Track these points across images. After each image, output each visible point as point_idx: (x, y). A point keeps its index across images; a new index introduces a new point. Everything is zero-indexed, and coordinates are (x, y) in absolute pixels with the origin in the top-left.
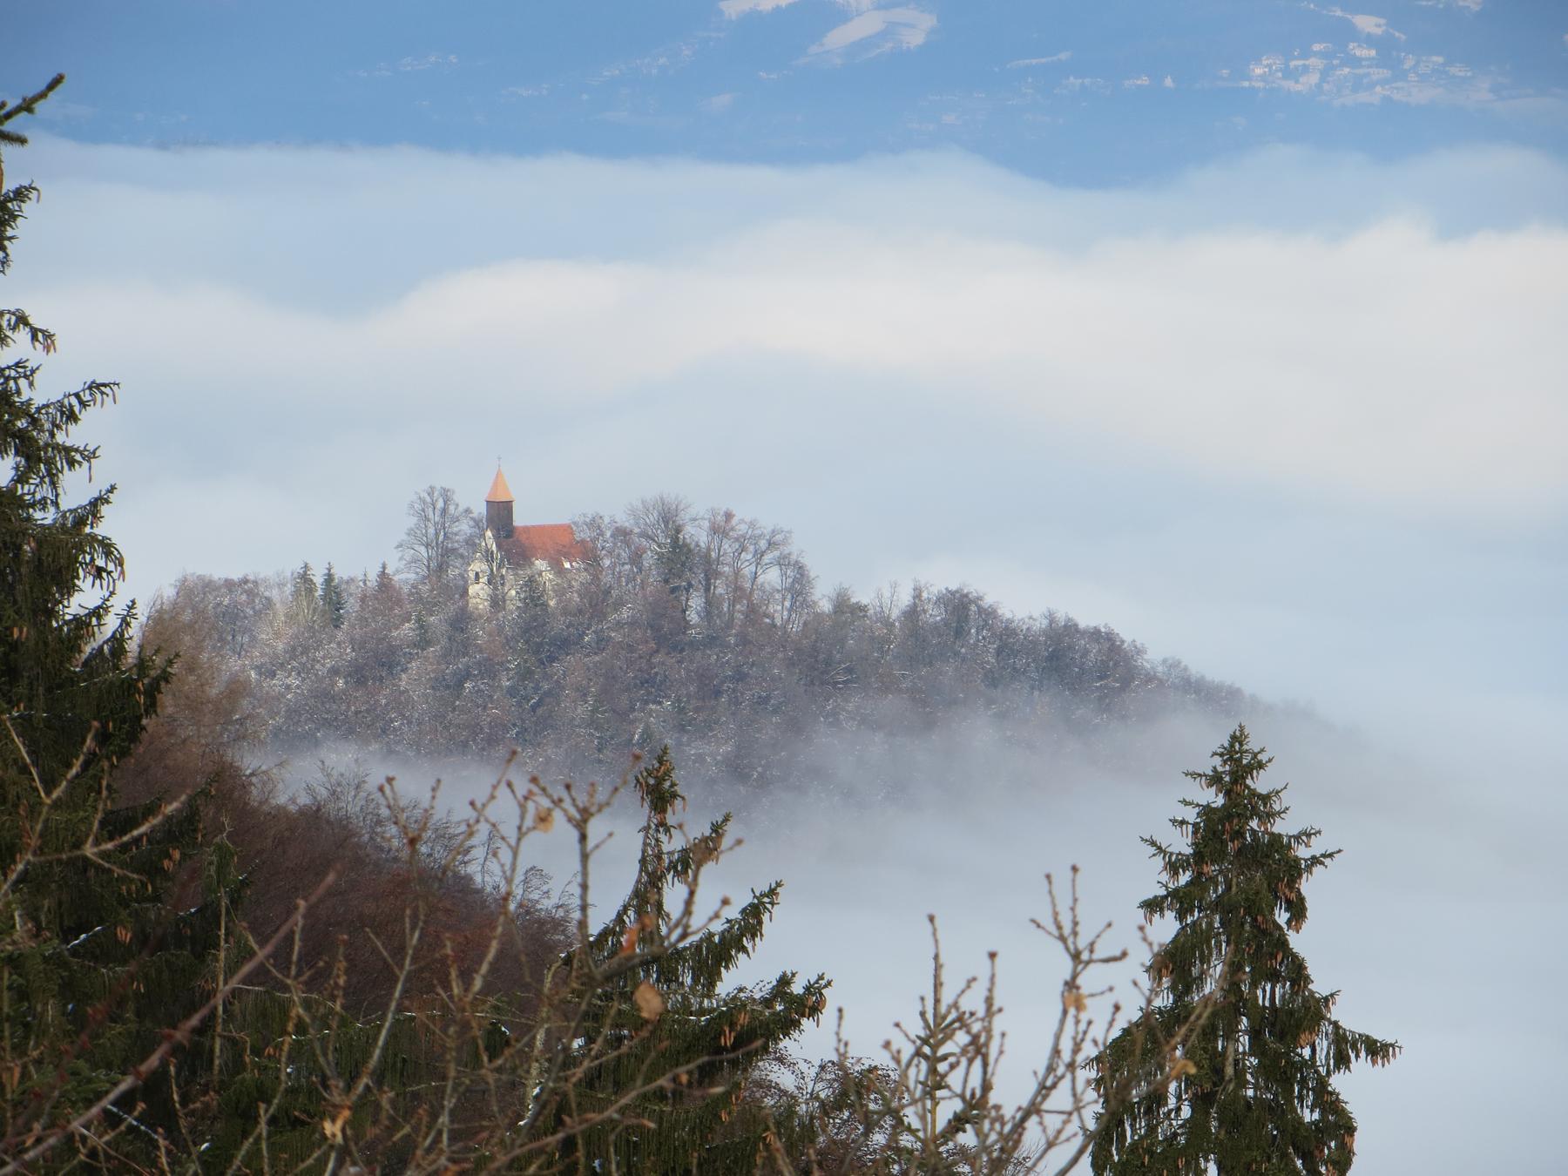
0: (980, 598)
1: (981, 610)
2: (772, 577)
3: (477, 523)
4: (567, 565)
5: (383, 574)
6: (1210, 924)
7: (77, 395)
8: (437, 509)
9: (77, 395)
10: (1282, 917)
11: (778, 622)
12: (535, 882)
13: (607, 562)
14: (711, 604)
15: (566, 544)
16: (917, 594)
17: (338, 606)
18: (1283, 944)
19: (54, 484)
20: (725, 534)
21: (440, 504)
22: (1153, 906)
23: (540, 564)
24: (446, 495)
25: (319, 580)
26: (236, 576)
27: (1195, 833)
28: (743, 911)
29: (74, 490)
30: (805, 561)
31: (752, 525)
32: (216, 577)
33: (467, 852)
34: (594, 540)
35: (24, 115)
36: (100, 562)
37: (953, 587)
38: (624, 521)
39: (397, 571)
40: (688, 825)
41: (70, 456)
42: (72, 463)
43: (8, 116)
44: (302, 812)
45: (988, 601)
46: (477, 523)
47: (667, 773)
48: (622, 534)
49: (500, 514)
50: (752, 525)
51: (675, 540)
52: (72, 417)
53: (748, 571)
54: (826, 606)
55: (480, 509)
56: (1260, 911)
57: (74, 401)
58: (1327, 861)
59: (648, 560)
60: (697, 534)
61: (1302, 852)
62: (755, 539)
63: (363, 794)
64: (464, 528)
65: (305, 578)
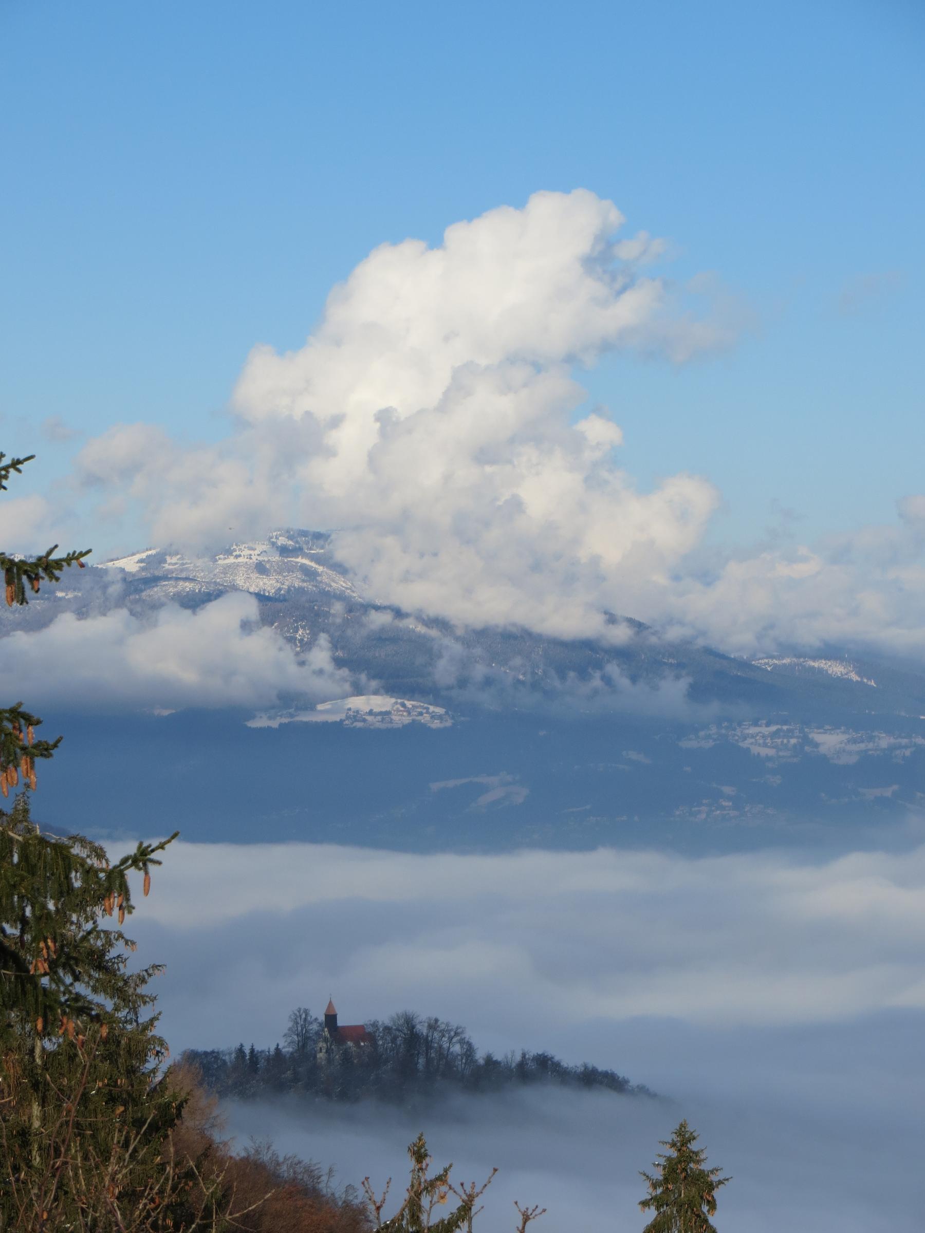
0: (552, 1058)
1: (553, 1063)
2: (457, 1049)
3: (320, 1024)
4: (362, 1044)
5: (277, 1049)
6: (672, 1212)
7: (146, 971)
8: (302, 1018)
9: (146, 971)
10: (705, 1208)
11: (460, 1069)
12: (350, 1191)
13: (381, 1042)
14: (429, 1061)
15: (359, 1033)
16: (524, 1055)
17: (256, 1063)
18: (706, 1221)
19: (136, 1014)
20: (435, 1029)
21: (303, 1016)
22: (645, 1204)
23: (350, 1044)
24: (306, 1012)
25: (247, 1051)
26: (209, 1050)
27: (664, 1169)
28: (458, 1209)
29: (145, 1014)
30: (471, 1041)
31: (447, 1025)
32: (200, 1050)
33: (319, 1177)
34: (375, 1032)
35: (160, 850)
36: (158, 1049)
37: (540, 1053)
38: (388, 1022)
39: (284, 1047)
40: (433, 1169)
41: (144, 999)
42: (145, 1003)
43: (153, 851)
44: (242, 1159)
45: (556, 1059)
46: (320, 1024)
47: (423, 1145)
48: (387, 1029)
49: (331, 1018)
50: (447, 1025)
51: (412, 1032)
52: (143, 981)
53: (446, 1046)
54: (481, 1062)
55: (322, 1018)
56: (695, 1206)
57: (145, 973)
58: (726, 1182)
59: (399, 1041)
60: (422, 1029)
61: (714, 1178)
62: (449, 1031)
63: (270, 1152)
64: (315, 1027)
65: (240, 1051)
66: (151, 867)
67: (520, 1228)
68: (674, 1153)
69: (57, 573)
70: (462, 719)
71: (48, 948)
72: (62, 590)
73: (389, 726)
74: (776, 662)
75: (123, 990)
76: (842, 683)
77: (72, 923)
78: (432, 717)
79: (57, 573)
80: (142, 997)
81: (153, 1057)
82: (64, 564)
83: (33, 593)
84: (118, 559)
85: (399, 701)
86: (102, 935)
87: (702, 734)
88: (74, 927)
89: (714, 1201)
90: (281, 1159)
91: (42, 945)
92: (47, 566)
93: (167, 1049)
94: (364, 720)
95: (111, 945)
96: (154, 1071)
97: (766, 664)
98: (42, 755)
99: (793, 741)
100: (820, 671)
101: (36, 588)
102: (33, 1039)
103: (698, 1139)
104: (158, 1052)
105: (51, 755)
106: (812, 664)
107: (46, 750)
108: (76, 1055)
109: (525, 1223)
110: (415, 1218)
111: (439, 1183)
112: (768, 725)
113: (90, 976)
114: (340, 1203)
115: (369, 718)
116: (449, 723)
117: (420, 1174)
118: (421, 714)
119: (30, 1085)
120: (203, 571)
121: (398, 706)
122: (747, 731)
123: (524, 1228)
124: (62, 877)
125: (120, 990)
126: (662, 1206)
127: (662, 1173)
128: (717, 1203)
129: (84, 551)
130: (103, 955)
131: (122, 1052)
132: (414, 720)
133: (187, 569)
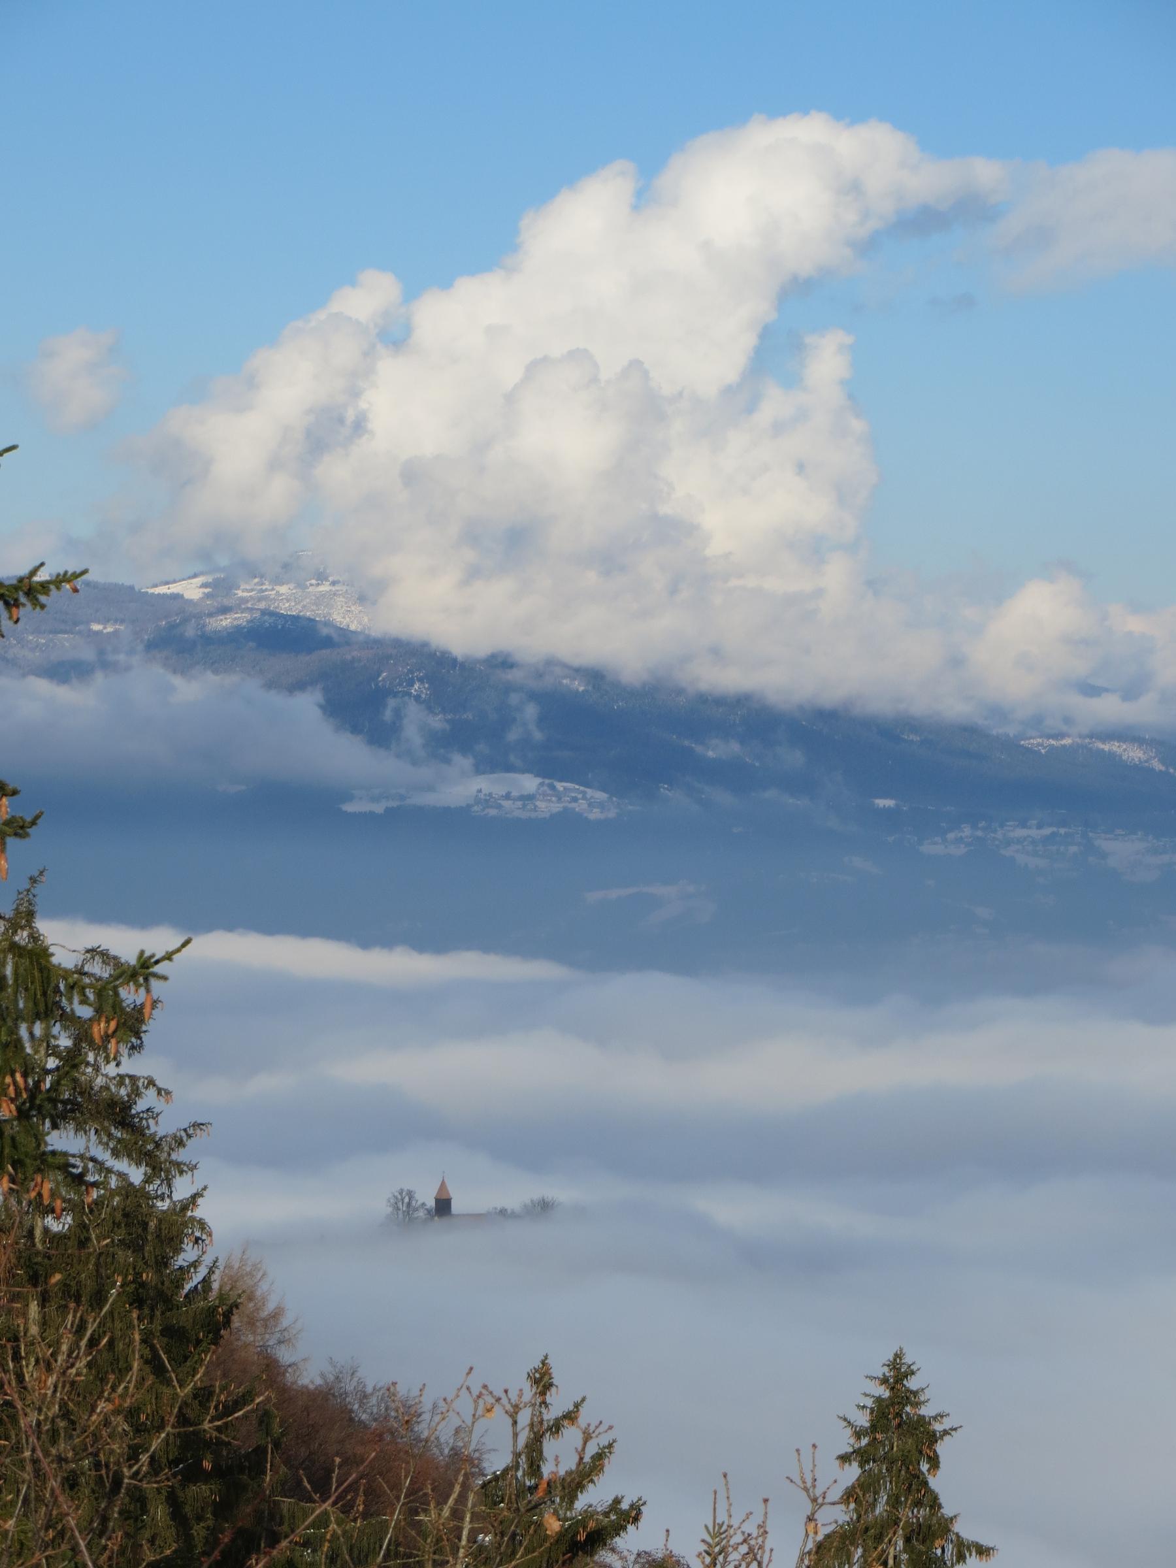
3: (429, 1211)
6: (880, 1470)
7: (185, 1130)
9: (185, 1130)
10: (924, 1467)
18: (926, 1483)
19: (170, 1186)
21: (406, 1200)
22: (844, 1458)
24: (410, 1194)
29: (182, 1188)
33: (420, 1415)
36: (198, 1234)
42: (181, 1172)
43: (157, 962)
52: (181, 1143)
55: (431, 1203)
56: (911, 1463)
57: (183, 1134)
58: (953, 1433)
61: (938, 1427)
63: (356, 1379)
66: (154, 982)
67: (580, 1449)
68: (886, 1394)
69: (43, 598)
70: (630, 807)
71: (15, 1083)
72: (99, 622)
73: (533, 815)
74: (1052, 742)
75: (156, 1157)
76: (1139, 769)
77: (88, 1064)
78: (590, 805)
79: (43, 598)
80: (178, 1164)
81: (191, 1245)
82: (52, 587)
83: (10, 623)
84: (175, 582)
85: (547, 781)
86: (127, 1081)
87: (951, 836)
88: (90, 1070)
89: (937, 1457)
90: (369, 1390)
91: (8, 1080)
92: (30, 589)
93: (210, 1235)
94: (500, 807)
95: (138, 1095)
96: (195, 1264)
97: (1039, 745)
98: (16, 834)
99: (1074, 849)
100: (1112, 755)
101: (15, 618)
102: (33, 1218)
103: (918, 1374)
104: (197, 1240)
105: (27, 835)
106: (1101, 746)
107: (22, 827)
108: (88, 1239)
109: (585, 1443)
110: (534, 1469)
111: (566, 1423)
112: (1039, 827)
113: (110, 1135)
114: (446, 1451)
115: (507, 804)
116: (612, 814)
117: (543, 1410)
118: (575, 800)
119: (26, 1278)
120: (288, 601)
121: (546, 788)
122: (1011, 835)
123: (584, 1449)
124: (39, 993)
125: (149, 1154)
126: (867, 1462)
127: (868, 1418)
128: (941, 1459)
129: (78, 571)
130: (130, 1108)
131: (149, 1238)
132: (565, 809)
133: (266, 598)
